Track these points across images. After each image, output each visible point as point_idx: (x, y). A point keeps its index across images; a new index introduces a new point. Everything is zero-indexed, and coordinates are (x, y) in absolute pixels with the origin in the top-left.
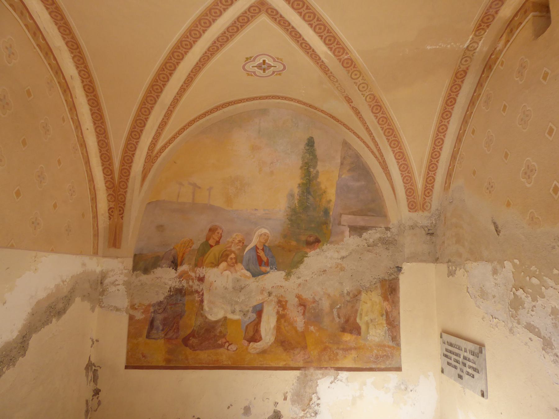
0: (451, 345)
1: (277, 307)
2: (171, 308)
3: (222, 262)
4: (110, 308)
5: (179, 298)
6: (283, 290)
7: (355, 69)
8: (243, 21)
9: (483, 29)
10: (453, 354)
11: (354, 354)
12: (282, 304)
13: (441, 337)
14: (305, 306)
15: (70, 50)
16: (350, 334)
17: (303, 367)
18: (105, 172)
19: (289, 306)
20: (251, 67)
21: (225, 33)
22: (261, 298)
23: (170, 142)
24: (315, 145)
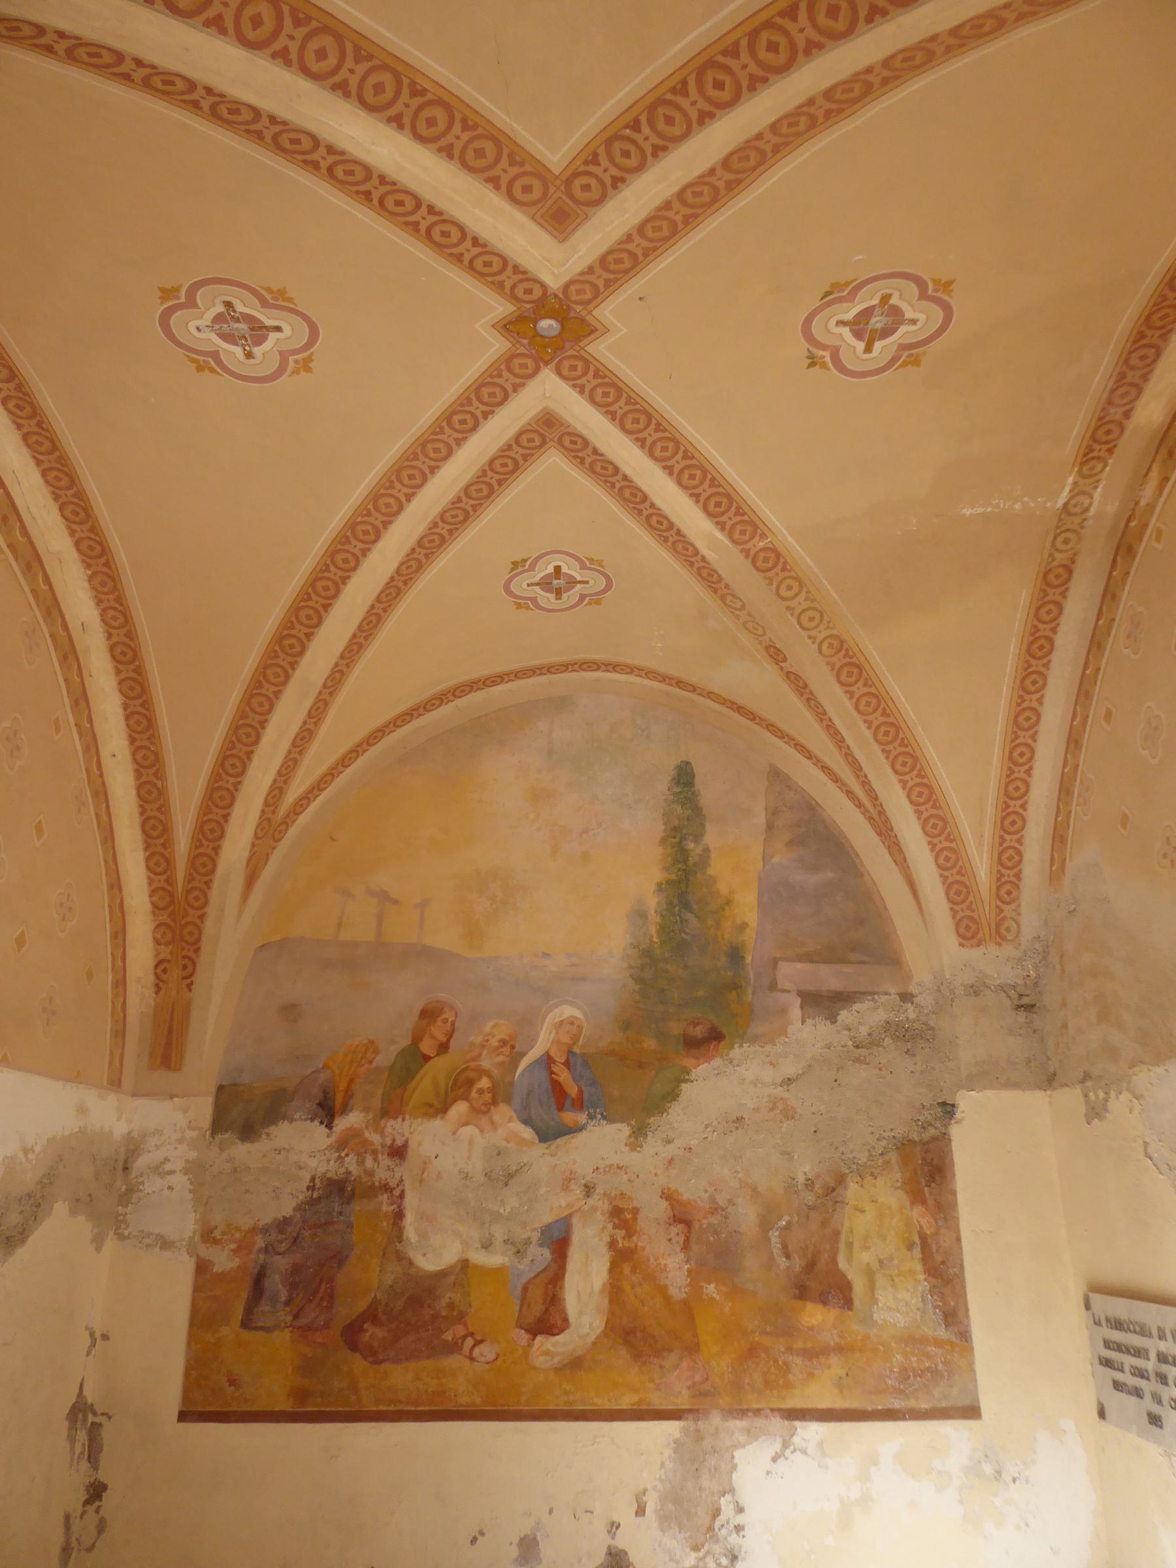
0: (1118, 1325)
1: (610, 1227)
2: (315, 1235)
3: (455, 1101)
4: (146, 1241)
5: (337, 1207)
6: (626, 1177)
7: (786, 574)
8: (504, 470)
9: (1098, 458)
10: (1128, 1352)
11: (836, 1366)
12: (622, 1217)
13: (1088, 1307)
14: (688, 1223)
15: (83, 561)
16: (820, 1307)
17: (690, 1411)
18: (152, 864)
19: (642, 1223)
20: (524, 585)
21: (459, 499)
22: (563, 1204)
23: (319, 787)
24: (697, 781)
